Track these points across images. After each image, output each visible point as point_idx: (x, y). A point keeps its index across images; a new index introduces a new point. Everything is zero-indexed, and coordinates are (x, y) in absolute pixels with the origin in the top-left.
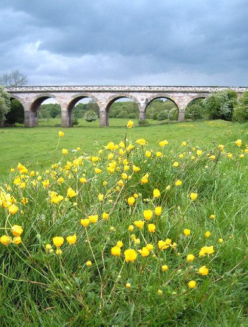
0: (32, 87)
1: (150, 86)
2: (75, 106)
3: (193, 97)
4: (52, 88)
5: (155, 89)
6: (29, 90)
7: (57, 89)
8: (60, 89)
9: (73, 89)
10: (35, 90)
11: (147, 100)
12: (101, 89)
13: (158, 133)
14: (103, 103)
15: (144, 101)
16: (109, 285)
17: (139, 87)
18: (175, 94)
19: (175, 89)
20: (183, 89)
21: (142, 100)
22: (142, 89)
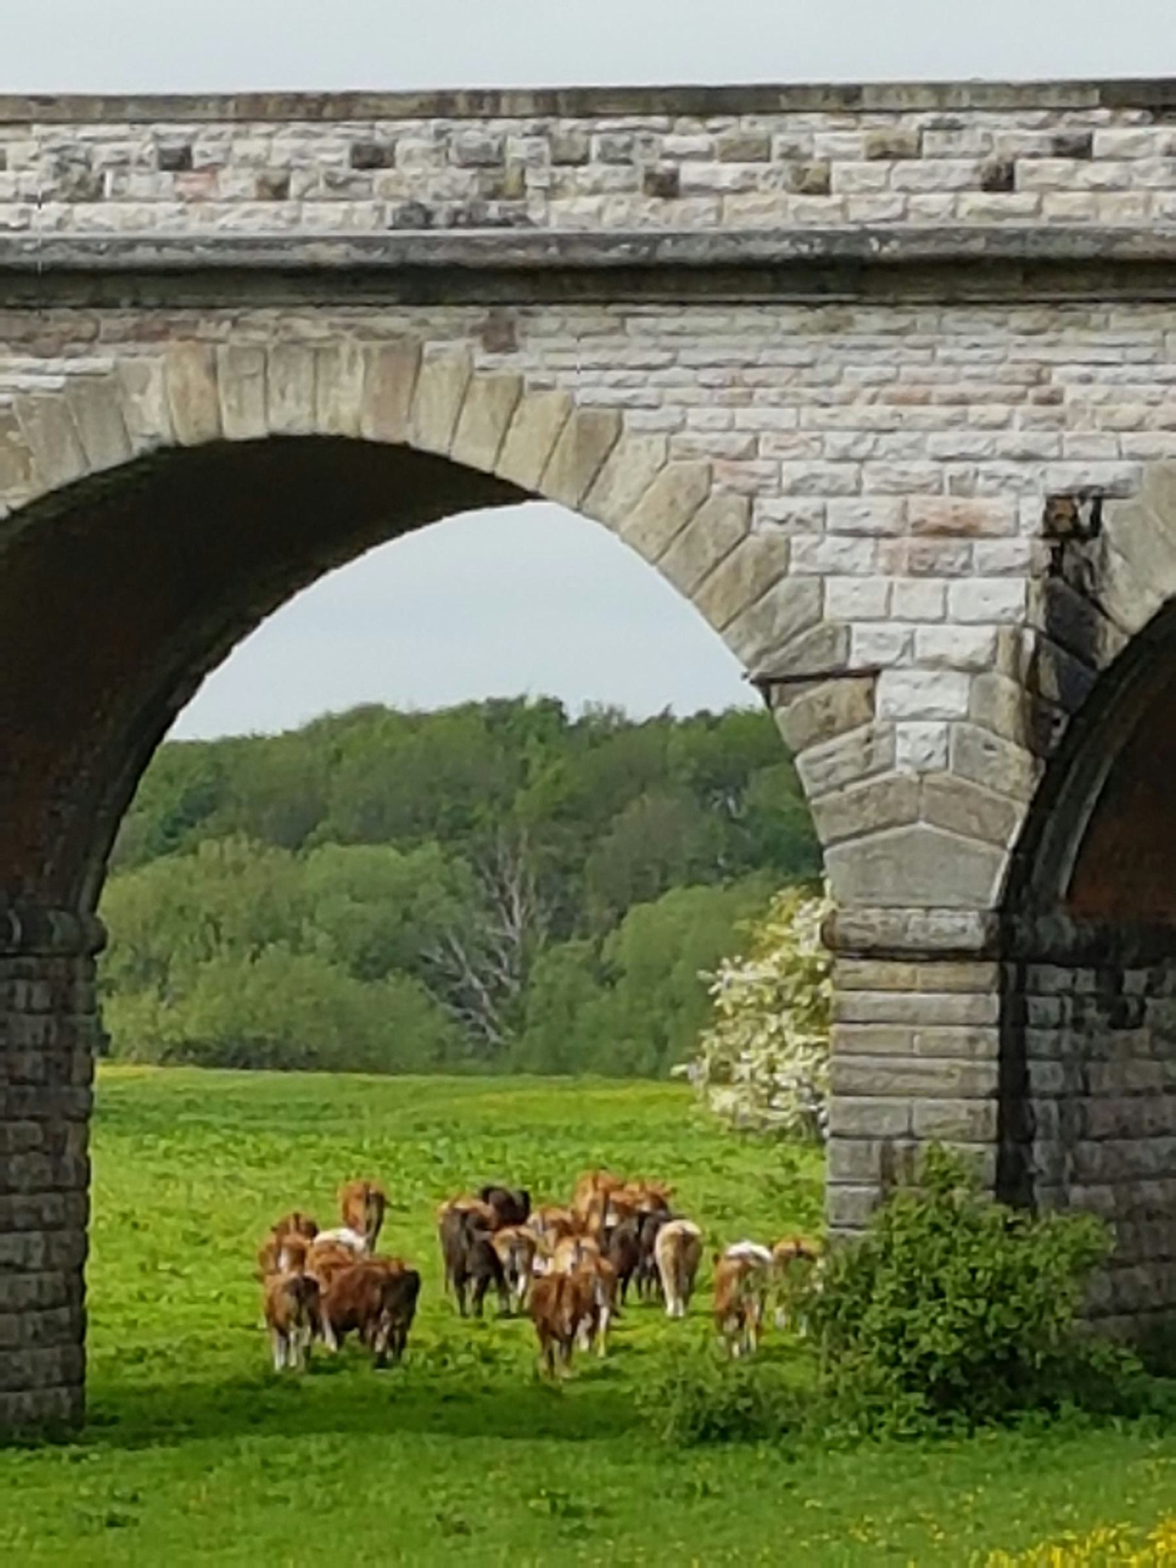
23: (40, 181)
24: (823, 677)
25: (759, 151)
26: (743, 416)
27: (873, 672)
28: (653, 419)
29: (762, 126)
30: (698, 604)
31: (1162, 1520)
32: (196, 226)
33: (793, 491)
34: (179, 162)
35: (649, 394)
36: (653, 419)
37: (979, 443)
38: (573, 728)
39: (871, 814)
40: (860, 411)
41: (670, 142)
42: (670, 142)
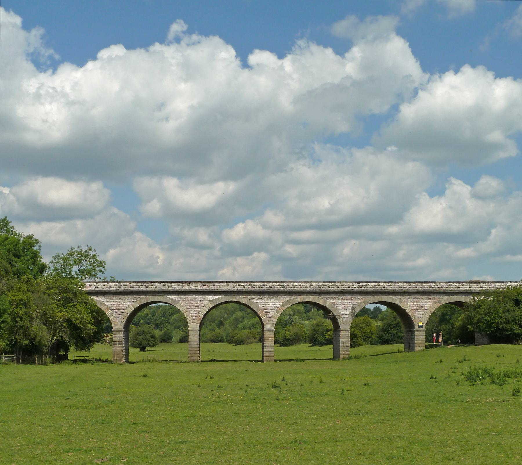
0: (130, 283)
1: (358, 283)
2: (150, 306)
3: (439, 301)
4: (169, 284)
5: (370, 287)
6: (123, 288)
7: (179, 287)
8: (186, 287)
9: (213, 288)
10: (136, 288)
11: (354, 307)
12: (267, 287)
13: (9, 279)
14: (270, 315)
15: (349, 311)
16: (96, 409)
17: (157, 284)
18: (407, 298)
19: (407, 287)
20: (420, 287)
21: (345, 308)
22: (345, 287)
23: (425, 196)
24: (339, 315)
25: (335, 285)
26: (334, 300)
27: (342, 315)
28: (329, 300)
29: (335, 284)
30: (39, 364)
31: (66, 288)
32: (301, 289)
33: (337, 305)
34: (300, 285)
35: (329, 299)
36: (329, 300)
37: (348, 302)
38: (372, 312)
39: (343, 323)
40: (341, 300)
41: (330, 285)
42: (330, 285)
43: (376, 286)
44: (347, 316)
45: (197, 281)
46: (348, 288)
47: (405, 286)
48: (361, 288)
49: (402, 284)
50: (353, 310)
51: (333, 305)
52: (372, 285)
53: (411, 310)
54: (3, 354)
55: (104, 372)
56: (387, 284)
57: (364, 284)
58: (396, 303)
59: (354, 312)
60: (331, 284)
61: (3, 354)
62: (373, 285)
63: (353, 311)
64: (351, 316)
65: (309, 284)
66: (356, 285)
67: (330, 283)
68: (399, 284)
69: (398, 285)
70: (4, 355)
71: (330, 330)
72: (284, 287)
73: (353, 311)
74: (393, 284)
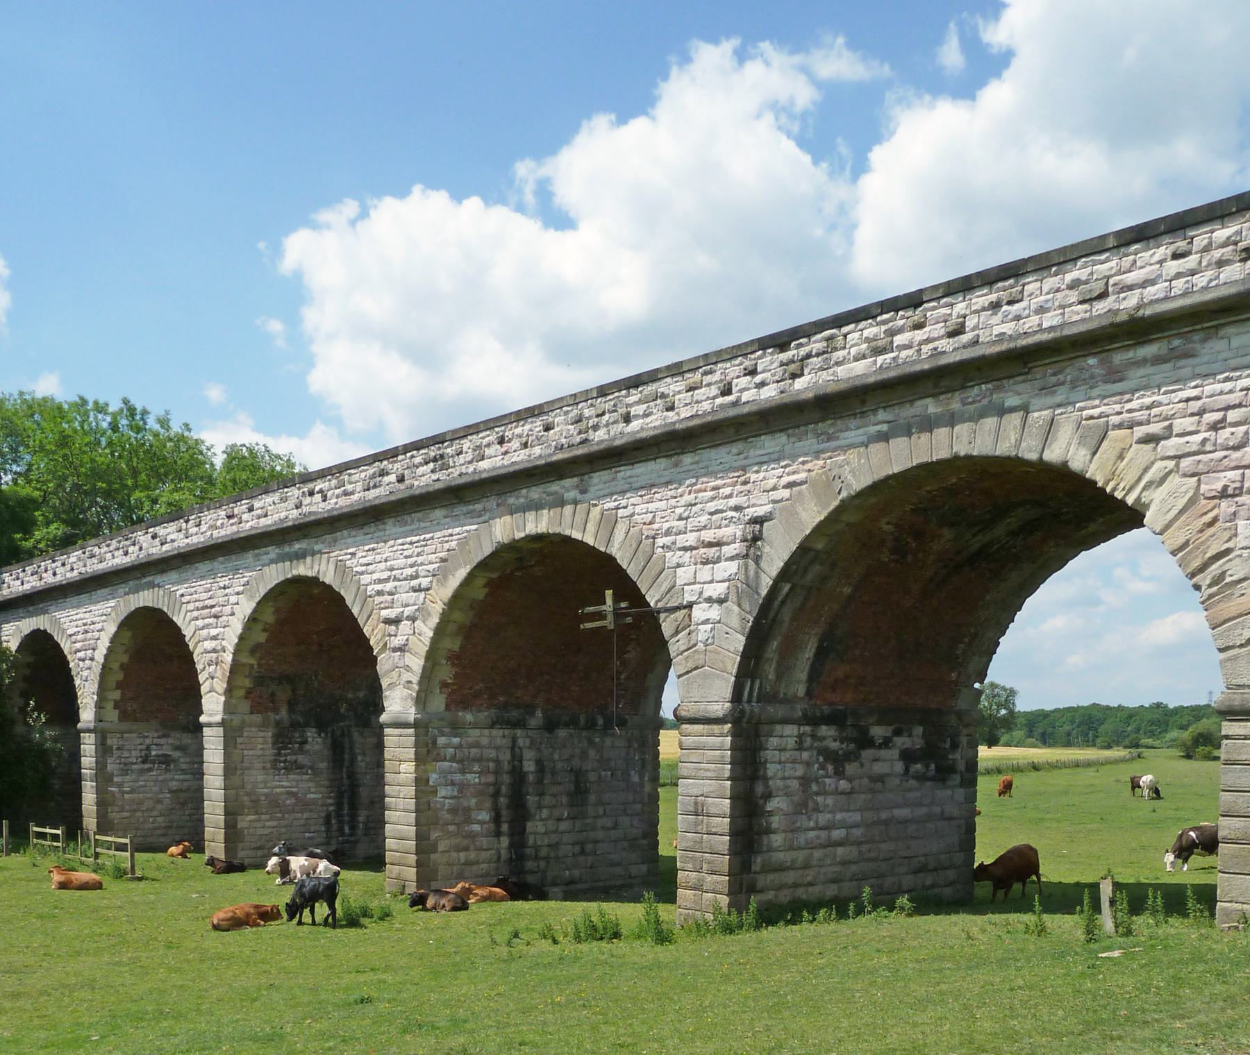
1: (780, 342)
43: (899, 340)
44: (714, 612)
45: (668, 368)
46: (719, 401)
47: (1131, 278)
48: (799, 384)
49: (1106, 266)
50: (751, 563)
51: (644, 543)
52: (866, 333)
53: (1192, 502)
54: (609, 593)
55: (1182, 540)
56: (982, 298)
57: (817, 344)
58: (1053, 455)
59: (757, 576)
60: (635, 396)
61: (609, 593)
62: (874, 330)
63: (752, 573)
64: (739, 605)
65: (537, 425)
66: (770, 362)
67: (628, 388)
68: (1077, 272)
69: (1069, 277)
70: (604, 603)
71: (514, 740)
72: (445, 467)
73: (752, 573)
74: (1032, 285)
